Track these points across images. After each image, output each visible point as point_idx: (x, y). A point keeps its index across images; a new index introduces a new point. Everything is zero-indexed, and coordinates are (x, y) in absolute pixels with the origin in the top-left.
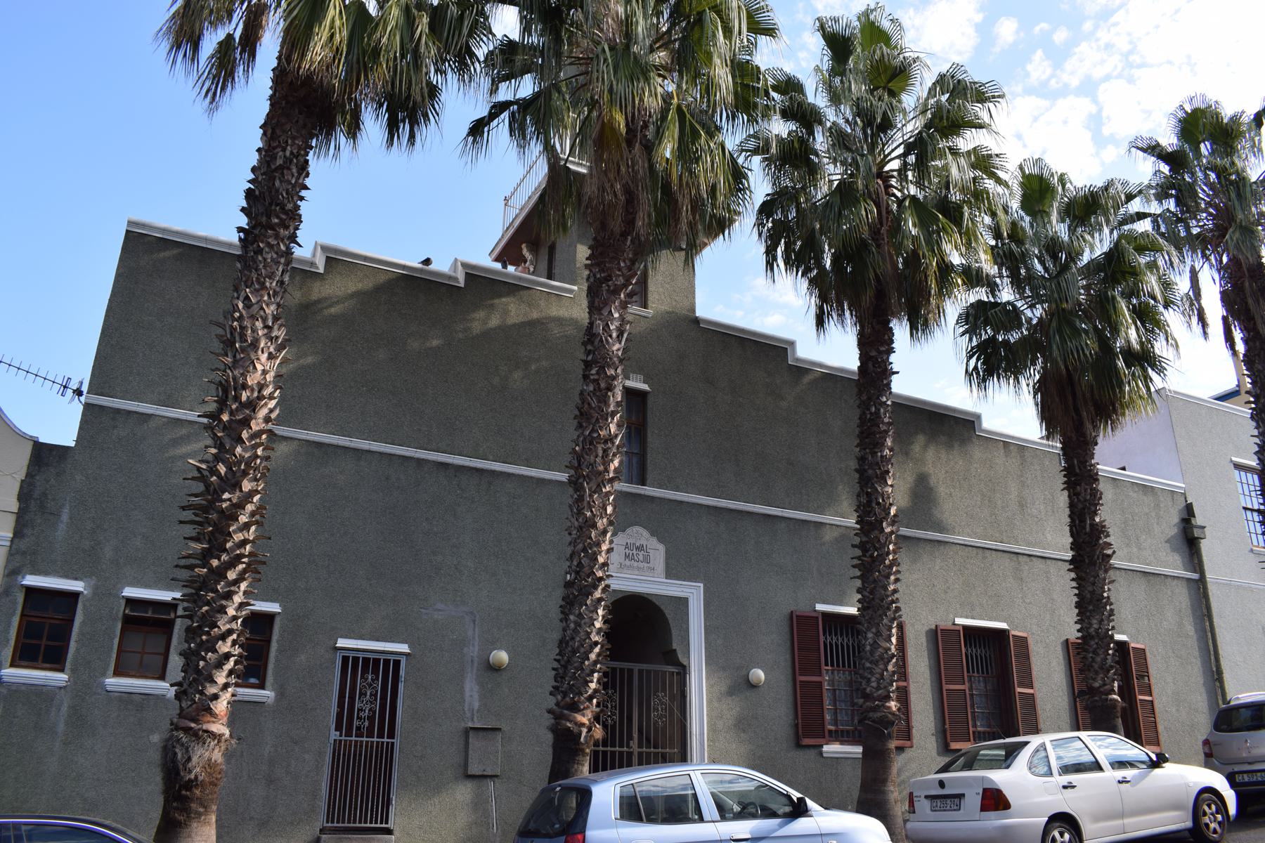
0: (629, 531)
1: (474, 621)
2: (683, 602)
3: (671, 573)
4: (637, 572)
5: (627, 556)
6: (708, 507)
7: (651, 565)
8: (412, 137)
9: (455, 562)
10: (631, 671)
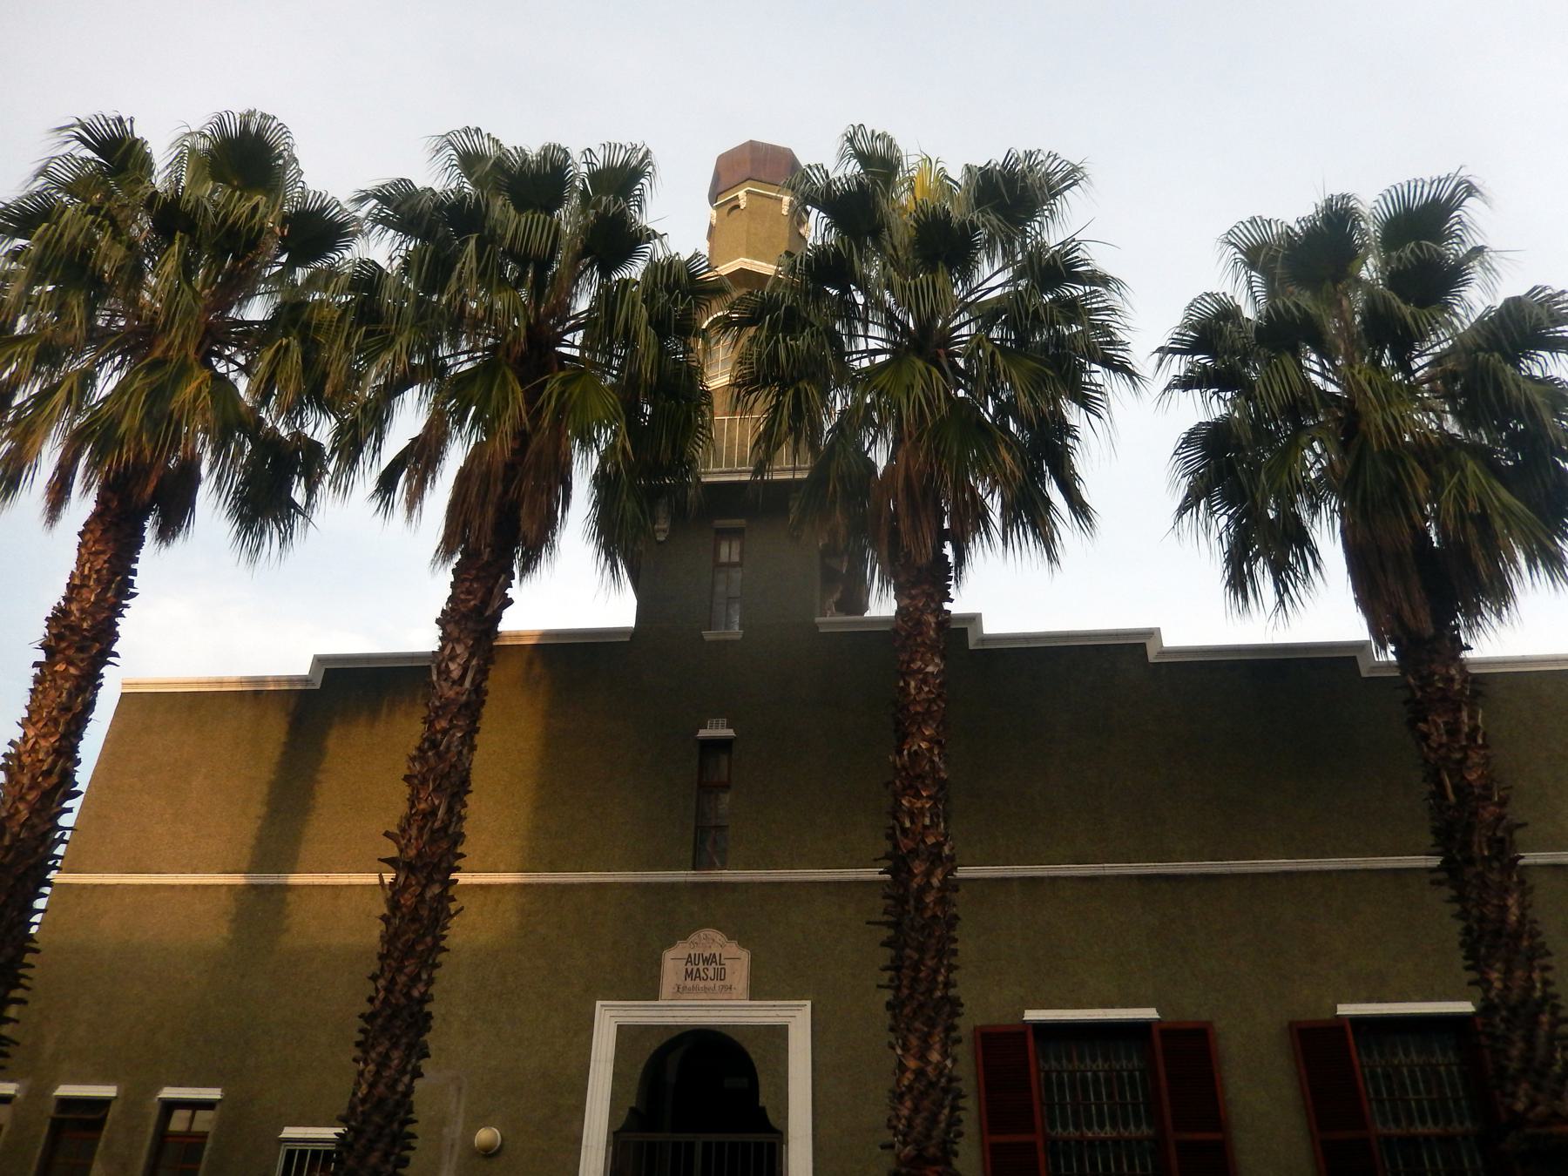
0: (694, 937)
1: (459, 1089)
2: (778, 1035)
3: (758, 990)
4: (704, 996)
5: (688, 974)
6: (826, 883)
7: (727, 982)
8: (1080, 508)
9: (443, 1012)
10: (690, 1146)
